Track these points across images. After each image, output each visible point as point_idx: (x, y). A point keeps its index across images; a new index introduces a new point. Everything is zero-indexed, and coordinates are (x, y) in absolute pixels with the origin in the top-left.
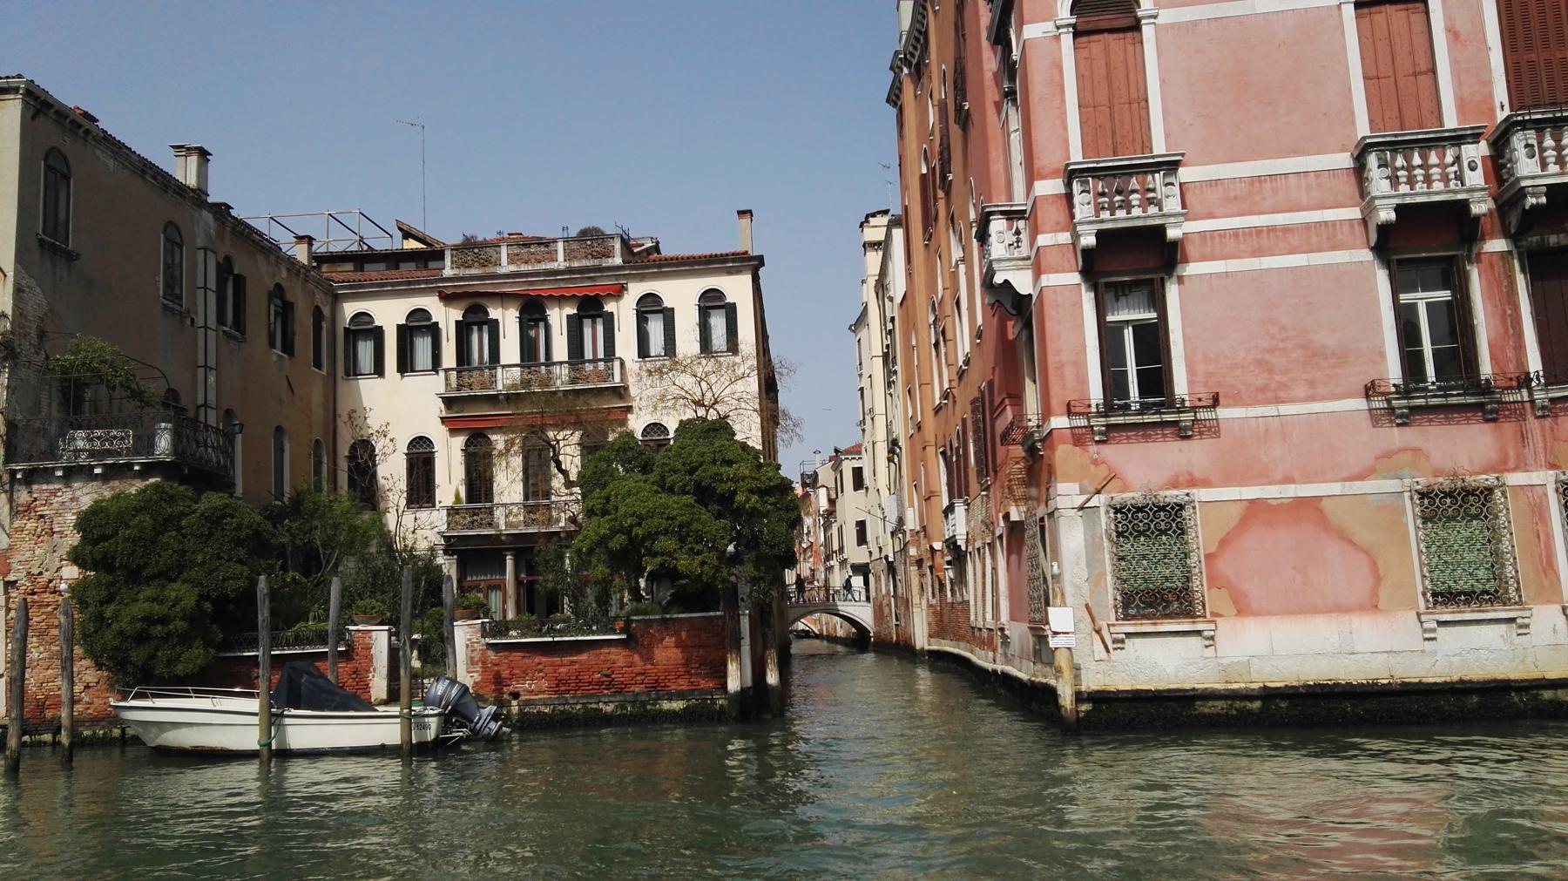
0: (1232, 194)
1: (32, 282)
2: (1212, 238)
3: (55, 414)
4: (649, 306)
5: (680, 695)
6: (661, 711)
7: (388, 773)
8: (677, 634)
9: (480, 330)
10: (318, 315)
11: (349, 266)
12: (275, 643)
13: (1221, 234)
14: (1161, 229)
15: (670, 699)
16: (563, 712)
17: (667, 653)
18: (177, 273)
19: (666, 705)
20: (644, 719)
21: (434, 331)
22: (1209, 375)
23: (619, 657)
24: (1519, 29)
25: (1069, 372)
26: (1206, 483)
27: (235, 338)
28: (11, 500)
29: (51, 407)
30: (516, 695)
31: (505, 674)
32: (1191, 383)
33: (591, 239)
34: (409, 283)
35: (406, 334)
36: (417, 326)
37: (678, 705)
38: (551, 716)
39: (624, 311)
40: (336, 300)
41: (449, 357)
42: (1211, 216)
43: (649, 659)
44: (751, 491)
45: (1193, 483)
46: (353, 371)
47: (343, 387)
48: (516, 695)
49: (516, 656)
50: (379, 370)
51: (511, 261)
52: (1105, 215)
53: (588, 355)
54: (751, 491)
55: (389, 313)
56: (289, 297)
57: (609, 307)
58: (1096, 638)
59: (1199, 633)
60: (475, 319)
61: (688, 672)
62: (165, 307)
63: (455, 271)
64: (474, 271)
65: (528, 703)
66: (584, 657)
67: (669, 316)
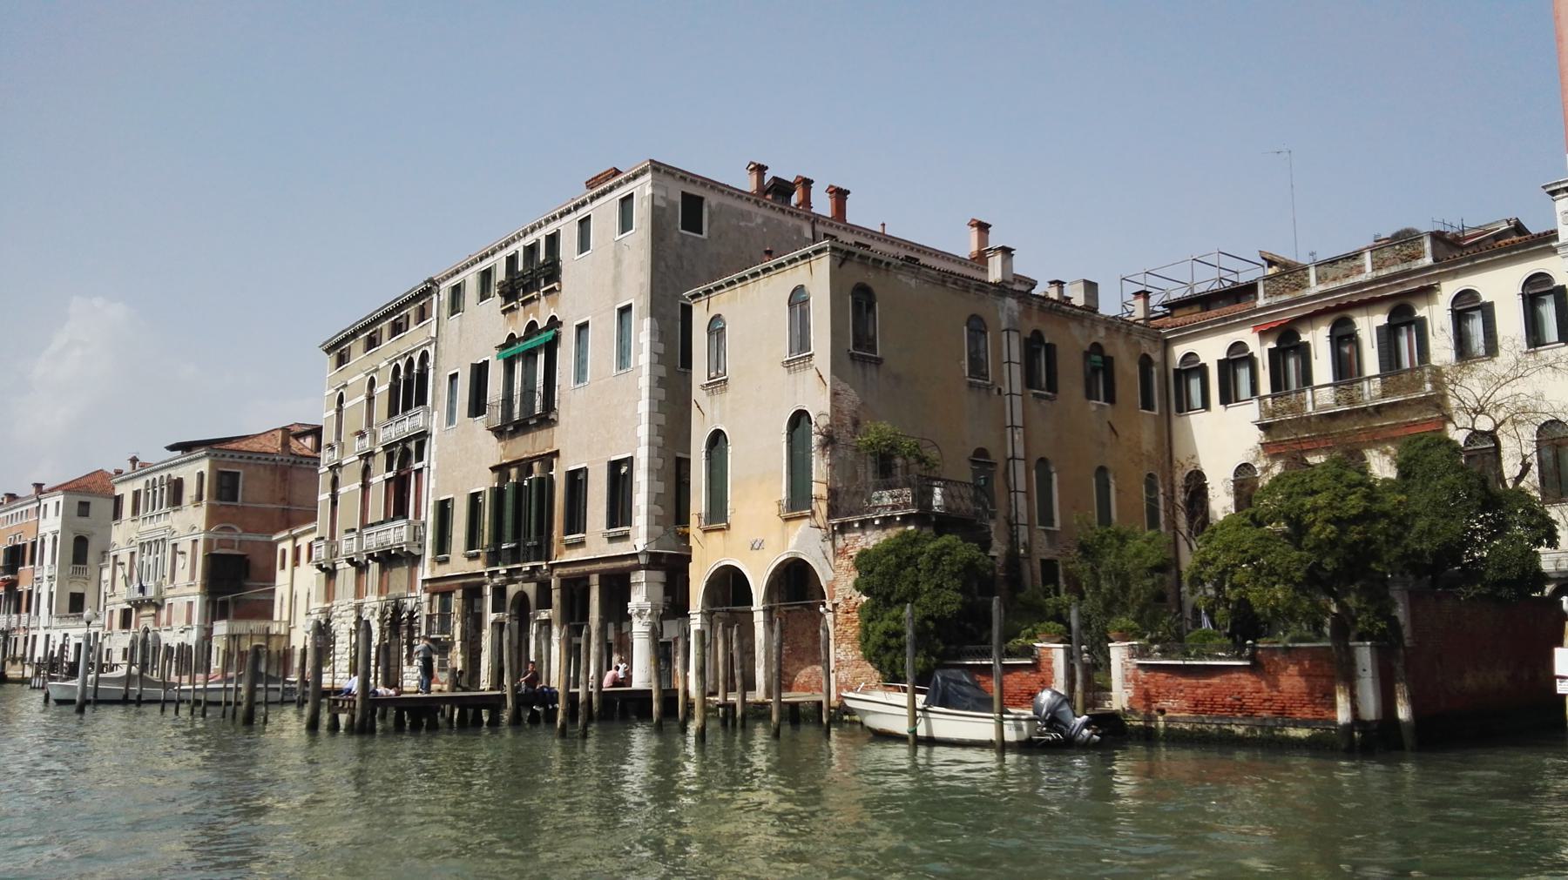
1: (846, 386)
3: (870, 479)
4: (1467, 307)
5: (1305, 724)
6: (1287, 738)
7: (989, 758)
8: (1299, 663)
9: (1409, 330)
10: (1146, 363)
12: (1002, 656)
15: (1295, 727)
16: (1201, 731)
17: (1291, 681)
18: (982, 356)
19: (1292, 732)
20: (1272, 745)
21: (1251, 361)
23: (1247, 682)
27: (1047, 397)
28: (834, 545)
29: (867, 473)
30: (1162, 712)
31: (1153, 691)
33: (1405, 240)
34: (1225, 319)
35: (1228, 367)
36: (1237, 359)
37: (1303, 733)
38: (1191, 733)
39: (1437, 314)
40: (1167, 345)
41: (1265, 387)
43: (1274, 685)
44: (1328, 521)
46: (1184, 406)
47: (1177, 422)
48: (1162, 712)
49: (1161, 676)
50: (1206, 405)
53: (1406, 364)
54: (1328, 521)
55: (1211, 350)
56: (1109, 352)
57: (1421, 312)
60: (1288, 344)
61: (1312, 702)
62: (971, 385)
64: (1285, 297)
65: (1171, 720)
66: (1216, 681)
67: (1488, 311)
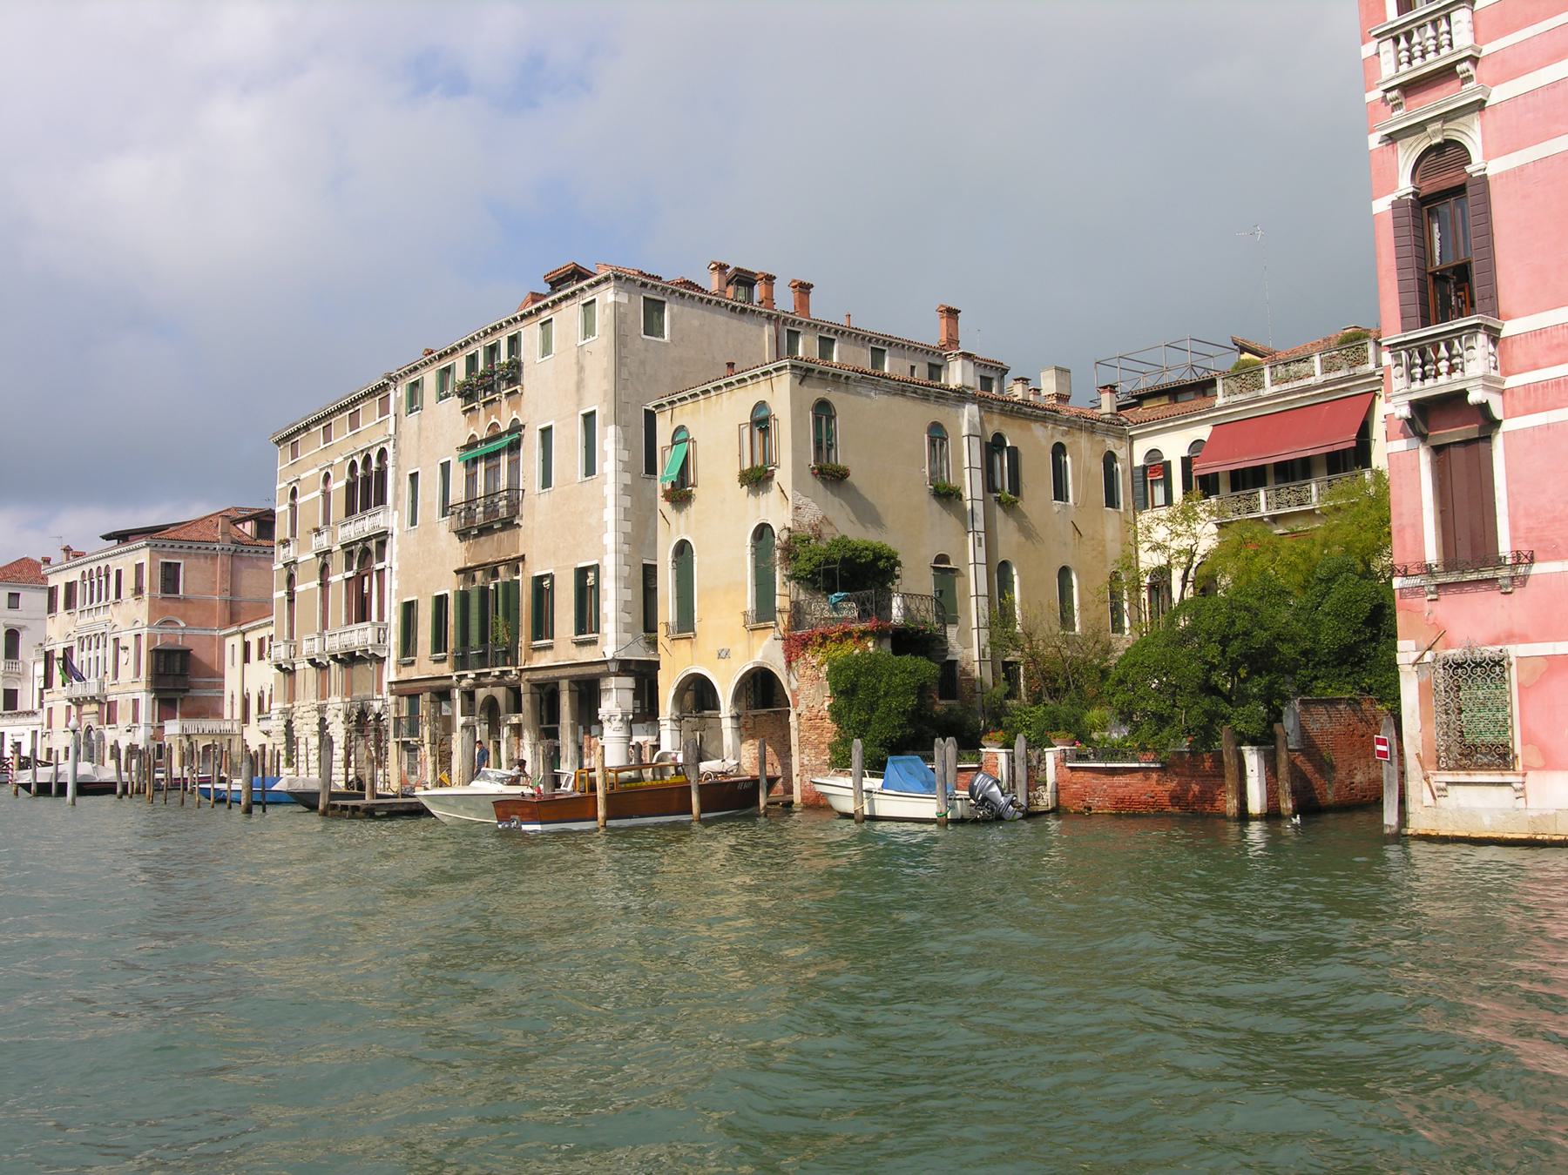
0: (1555, 341)
2: (1536, 389)
11: (1165, 400)
13: (1545, 385)
14: (1463, 394)
22: (1530, 530)
24: (1460, 225)
25: (1409, 535)
26: (1524, 639)
32: (1513, 539)
42: (1536, 367)
45: (1511, 638)
51: (1274, 382)
52: (1417, 385)
58: (1425, 784)
59: (1509, 784)
63: (1276, 389)
